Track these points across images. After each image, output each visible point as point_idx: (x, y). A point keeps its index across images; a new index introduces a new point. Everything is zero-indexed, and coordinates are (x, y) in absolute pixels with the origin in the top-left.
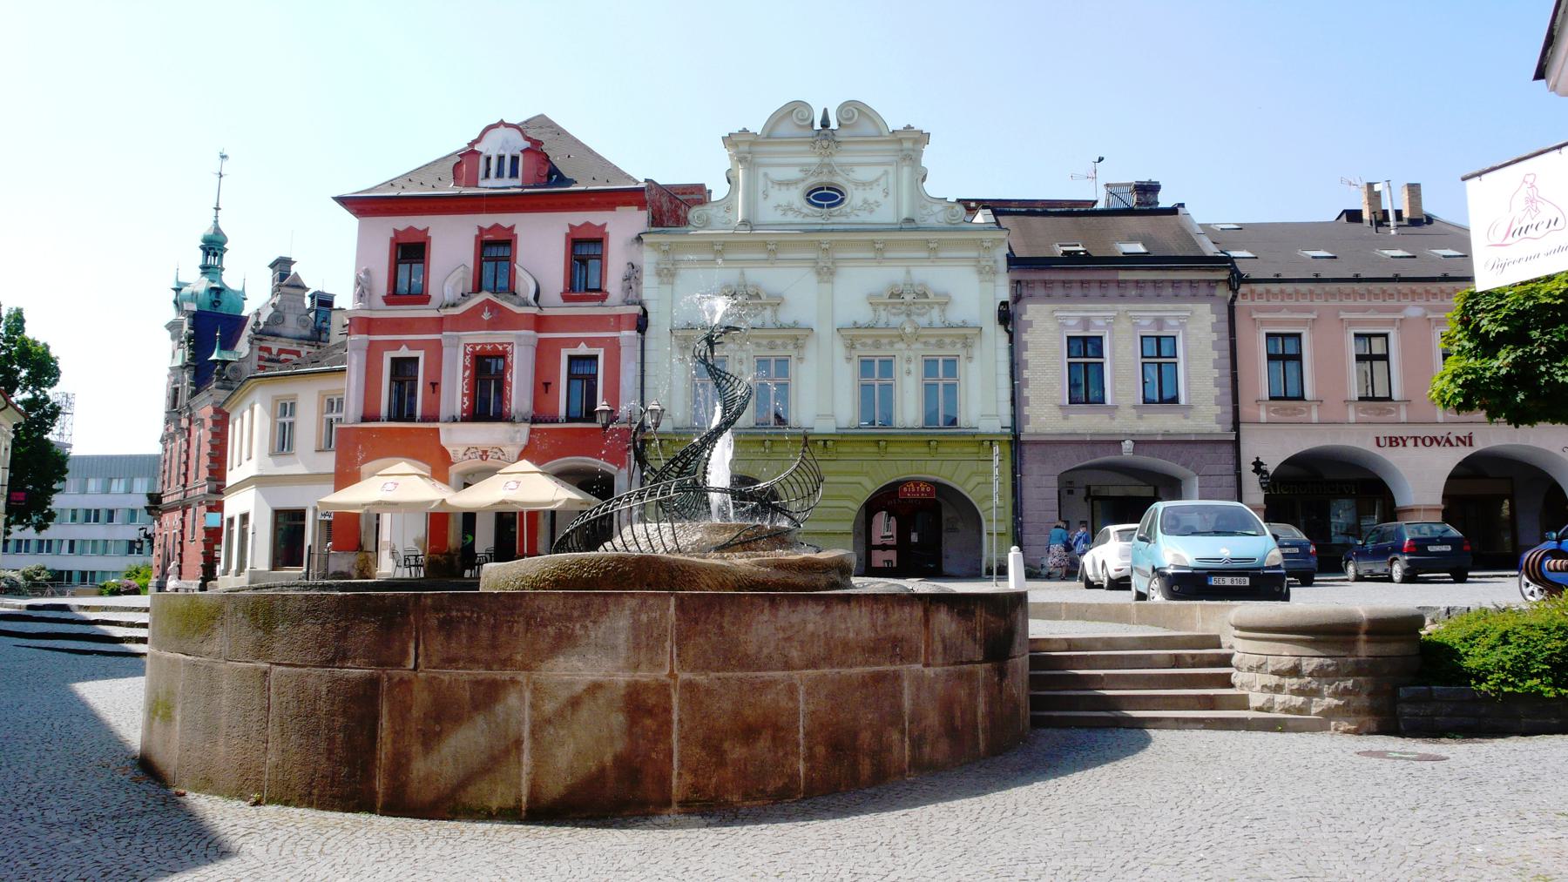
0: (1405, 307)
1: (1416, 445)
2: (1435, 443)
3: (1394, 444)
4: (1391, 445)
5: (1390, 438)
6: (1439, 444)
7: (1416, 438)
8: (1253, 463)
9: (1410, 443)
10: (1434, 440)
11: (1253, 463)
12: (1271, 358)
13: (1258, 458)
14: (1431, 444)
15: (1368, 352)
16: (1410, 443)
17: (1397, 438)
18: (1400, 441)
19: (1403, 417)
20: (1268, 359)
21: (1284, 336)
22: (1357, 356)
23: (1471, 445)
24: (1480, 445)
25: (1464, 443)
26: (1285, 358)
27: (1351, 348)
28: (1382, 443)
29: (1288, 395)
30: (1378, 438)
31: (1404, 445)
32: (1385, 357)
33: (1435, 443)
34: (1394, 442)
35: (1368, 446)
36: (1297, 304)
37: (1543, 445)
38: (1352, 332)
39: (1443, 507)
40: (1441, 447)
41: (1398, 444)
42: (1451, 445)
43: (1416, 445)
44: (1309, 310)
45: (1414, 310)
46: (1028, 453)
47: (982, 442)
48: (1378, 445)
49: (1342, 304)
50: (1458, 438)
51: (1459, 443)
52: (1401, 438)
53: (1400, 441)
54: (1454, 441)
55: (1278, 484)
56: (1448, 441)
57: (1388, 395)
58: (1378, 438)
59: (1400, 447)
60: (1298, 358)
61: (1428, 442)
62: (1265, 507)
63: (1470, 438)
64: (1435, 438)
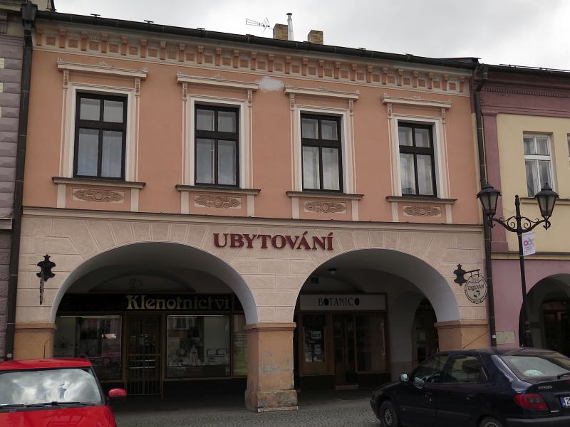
0: (261, 77)
1: (264, 246)
2: (288, 246)
3: (237, 244)
4: (233, 246)
5: (233, 236)
6: (292, 245)
7: (264, 238)
8: (40, 264)
9: (257, 244)
10: (287, 241)
11: (40, 264)
12: (200, 135)
13: (47, 257)
14: (283, 246)
15: (317, 138)
16: (257, 244)
17: (240, 237)
18: (244, 240)
19: (251, 212)
20: (303, 145)
21: (103, 97)
22: (401, 147)
23: (330, 248)
24: (340, 249)
25: (323, 246)
26: (101, 127)
27: (395, 138)
28: (221, 243)
29: (103, 175)
30: (216, 236)
31: (250, 246)
32: (121, 128)
33: (288, 246)
34: (237, 241)
35: (199, 240)
36: (235, 70)
37: (410, 251)
38: (191, 102)
39: (295, 325)
40: (295, 251)
41: (242, 245)
42: (308, 248)
43: (264, 246)
44: (138, 67)
45: (270, 83)
46: (525, 263)
47: (514, 253)
48: (217, 244)
49: (182, 64)
50: (316, 239)
51: (317, 246)
52: (247, 236)
53: (244, 240)
54: (310, 242)
55: (143, 297)
56: (304, 242)
57: (118, 175)
58: (216, 236)
59: (244, 249)
60: (234, 137)
61: (279, 243)
62: (295, 325)
63: (330, 240)
64: (289, 238)
